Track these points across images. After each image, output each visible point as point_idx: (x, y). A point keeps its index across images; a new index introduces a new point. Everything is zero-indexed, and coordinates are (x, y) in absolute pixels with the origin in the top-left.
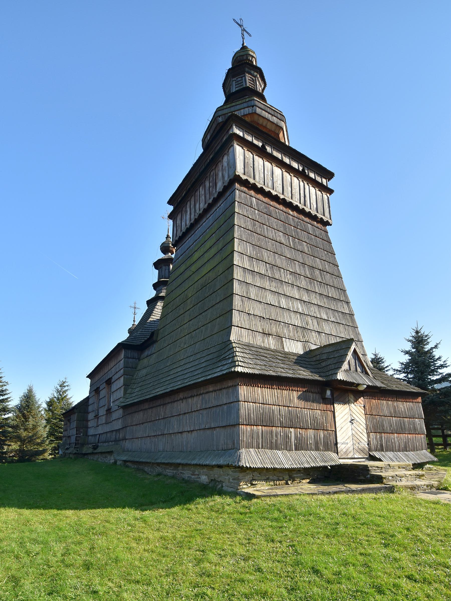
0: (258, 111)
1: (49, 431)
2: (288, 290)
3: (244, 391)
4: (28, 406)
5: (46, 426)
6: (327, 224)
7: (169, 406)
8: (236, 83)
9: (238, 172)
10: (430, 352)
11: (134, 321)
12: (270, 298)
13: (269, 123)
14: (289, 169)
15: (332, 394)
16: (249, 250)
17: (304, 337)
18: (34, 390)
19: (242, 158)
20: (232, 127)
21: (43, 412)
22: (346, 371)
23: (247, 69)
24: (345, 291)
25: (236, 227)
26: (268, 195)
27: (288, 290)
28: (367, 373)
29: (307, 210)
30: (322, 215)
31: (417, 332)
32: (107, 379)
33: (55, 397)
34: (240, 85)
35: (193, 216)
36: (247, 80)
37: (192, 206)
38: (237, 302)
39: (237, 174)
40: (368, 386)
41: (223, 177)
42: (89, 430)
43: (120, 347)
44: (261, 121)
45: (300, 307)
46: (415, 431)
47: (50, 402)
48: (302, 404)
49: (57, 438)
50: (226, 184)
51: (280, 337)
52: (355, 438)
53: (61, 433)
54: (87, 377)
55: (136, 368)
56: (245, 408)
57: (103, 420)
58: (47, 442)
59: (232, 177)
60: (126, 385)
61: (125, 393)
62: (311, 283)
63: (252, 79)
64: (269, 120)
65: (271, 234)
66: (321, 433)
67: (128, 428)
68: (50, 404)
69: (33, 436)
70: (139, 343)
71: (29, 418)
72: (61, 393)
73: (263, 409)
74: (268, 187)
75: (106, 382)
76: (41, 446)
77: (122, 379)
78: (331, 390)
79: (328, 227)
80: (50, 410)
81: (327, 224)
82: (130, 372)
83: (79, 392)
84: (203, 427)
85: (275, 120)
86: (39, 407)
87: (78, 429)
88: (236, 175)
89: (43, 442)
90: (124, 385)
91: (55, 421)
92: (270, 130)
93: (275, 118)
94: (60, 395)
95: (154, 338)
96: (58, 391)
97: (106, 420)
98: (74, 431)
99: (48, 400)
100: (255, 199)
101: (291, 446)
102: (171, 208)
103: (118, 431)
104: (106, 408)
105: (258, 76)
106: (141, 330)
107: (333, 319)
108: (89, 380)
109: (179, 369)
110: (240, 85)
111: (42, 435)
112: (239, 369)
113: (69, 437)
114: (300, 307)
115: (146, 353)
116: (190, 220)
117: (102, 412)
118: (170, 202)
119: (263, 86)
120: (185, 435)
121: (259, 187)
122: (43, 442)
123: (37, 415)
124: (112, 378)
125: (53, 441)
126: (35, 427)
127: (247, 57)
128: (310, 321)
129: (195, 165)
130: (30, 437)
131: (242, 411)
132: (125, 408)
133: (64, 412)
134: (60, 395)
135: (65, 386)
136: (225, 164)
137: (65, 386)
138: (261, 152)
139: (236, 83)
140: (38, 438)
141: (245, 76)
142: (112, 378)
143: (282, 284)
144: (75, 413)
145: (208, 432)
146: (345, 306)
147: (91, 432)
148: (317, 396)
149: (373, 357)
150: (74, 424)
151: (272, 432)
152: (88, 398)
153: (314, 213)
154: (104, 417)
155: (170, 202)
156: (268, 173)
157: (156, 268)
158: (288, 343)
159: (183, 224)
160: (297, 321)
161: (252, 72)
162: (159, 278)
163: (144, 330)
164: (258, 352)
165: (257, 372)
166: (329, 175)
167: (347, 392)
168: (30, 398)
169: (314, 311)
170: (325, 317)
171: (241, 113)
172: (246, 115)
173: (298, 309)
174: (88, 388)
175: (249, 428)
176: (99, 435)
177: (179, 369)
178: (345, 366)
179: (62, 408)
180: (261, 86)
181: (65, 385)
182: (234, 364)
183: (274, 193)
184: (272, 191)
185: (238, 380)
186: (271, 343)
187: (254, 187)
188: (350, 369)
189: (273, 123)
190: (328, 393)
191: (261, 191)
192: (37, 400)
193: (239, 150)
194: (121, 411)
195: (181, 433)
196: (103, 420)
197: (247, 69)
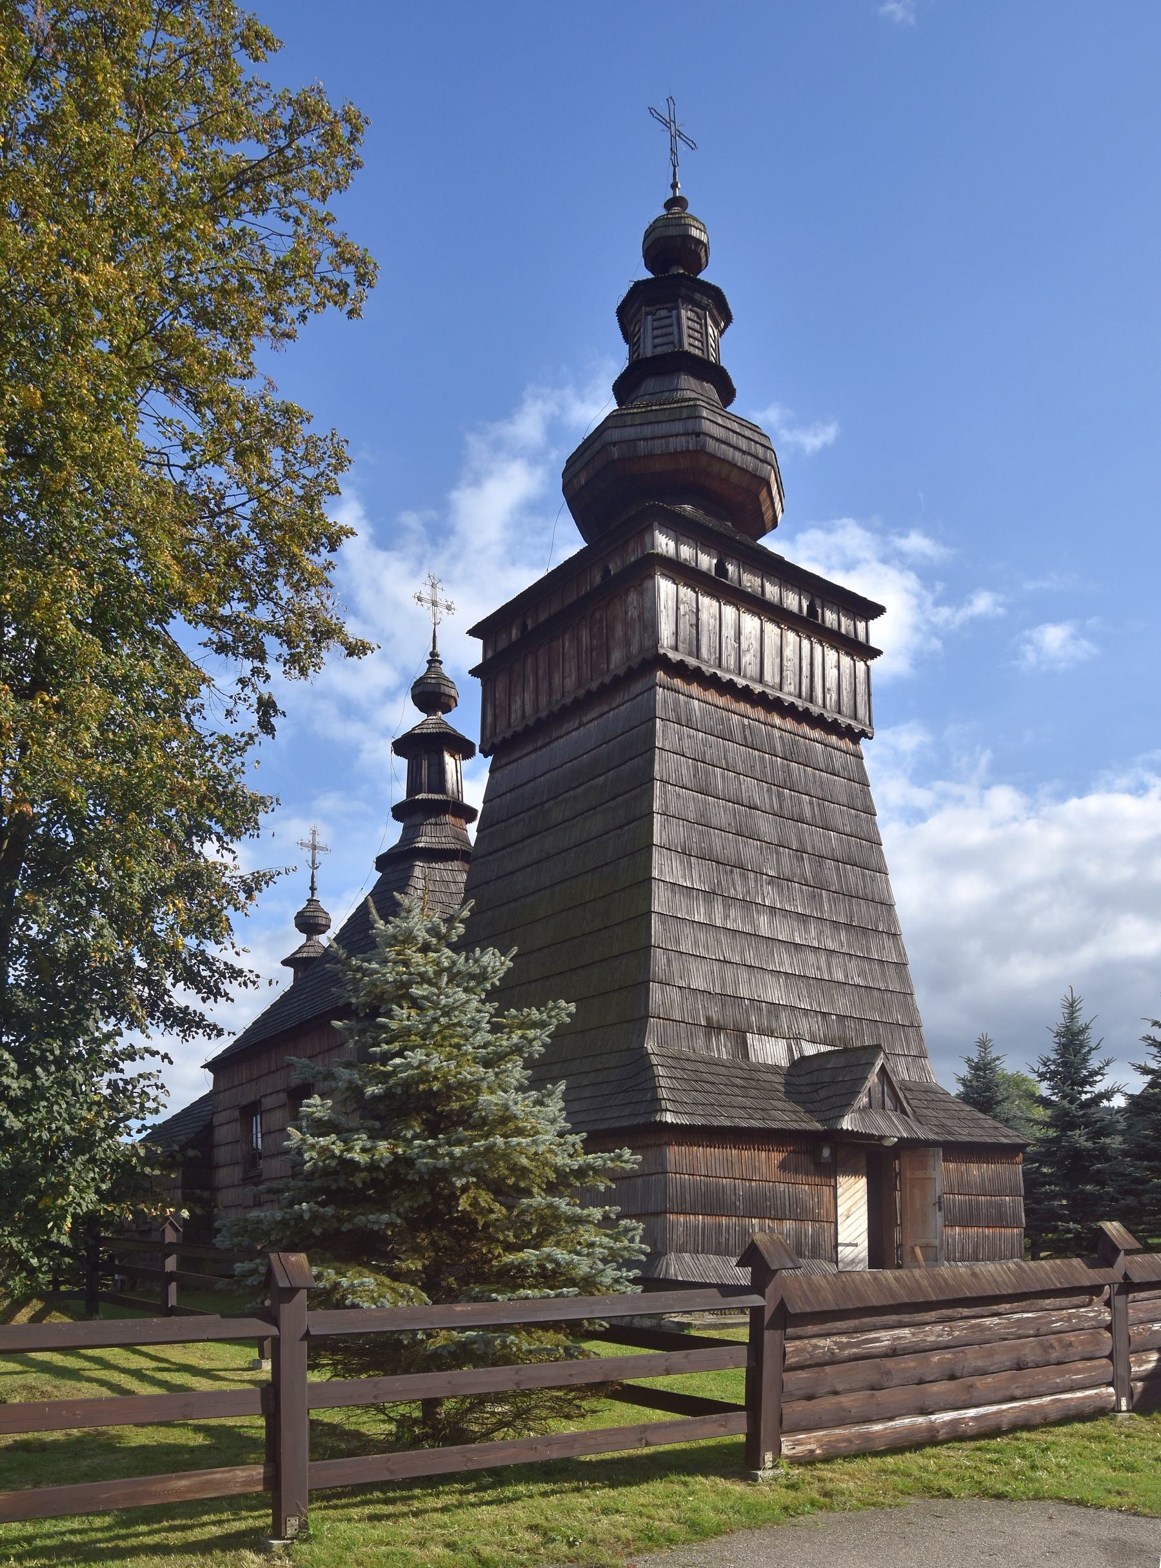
0: (711, 445)
6: (855, 736)
8: (656, 324)
9: (662, 647)
10: (1082, 1031)
11: (313, 889)
15: (834, 1154)
19: (672, 604)
22: (862, 1110)
23: (683, 291)
24: (890, 906)
28: (904, 1112)
29: (815, 710)
30: (850, 718)
34: (664, 331)
35: (543, 700)
36: (684, 321)
37: (541, 672)
39: (661, 651)
40: (901, 1139)
41: (628, 643)
46: (1000, 1220)
50: (635, 663)
64: (732, 465)
66: (809, 1228)
73: (706, 1185)
74: (728, 671)
78: (831, 1148)
85: (749, 463)
93: (749, 458)
100: (699, 702)
110: (664, 331)
112: (669, 1118)
116: (536, 708)
121: (708, 674)
131: (671, 1190)
136: (633, 613)
139: (656, 324)
141: (677, 308)
146: (888, 943)
153: (830, 716)
156: (728, 632)
159: (517, 706)
162: (413, 788)
164: (697, 1073)
165: (699, 1121)
170: (839, 976)
171: (668, 444)
172: (682, 452)
175: (682, 1218)
182: (655, 1105)
183: (741, 682)
184: (735, 679)
186: (721, 1049)
189: (745, 471)
190: (826, 1152)
193: (666, 588)
197: (683, 291)
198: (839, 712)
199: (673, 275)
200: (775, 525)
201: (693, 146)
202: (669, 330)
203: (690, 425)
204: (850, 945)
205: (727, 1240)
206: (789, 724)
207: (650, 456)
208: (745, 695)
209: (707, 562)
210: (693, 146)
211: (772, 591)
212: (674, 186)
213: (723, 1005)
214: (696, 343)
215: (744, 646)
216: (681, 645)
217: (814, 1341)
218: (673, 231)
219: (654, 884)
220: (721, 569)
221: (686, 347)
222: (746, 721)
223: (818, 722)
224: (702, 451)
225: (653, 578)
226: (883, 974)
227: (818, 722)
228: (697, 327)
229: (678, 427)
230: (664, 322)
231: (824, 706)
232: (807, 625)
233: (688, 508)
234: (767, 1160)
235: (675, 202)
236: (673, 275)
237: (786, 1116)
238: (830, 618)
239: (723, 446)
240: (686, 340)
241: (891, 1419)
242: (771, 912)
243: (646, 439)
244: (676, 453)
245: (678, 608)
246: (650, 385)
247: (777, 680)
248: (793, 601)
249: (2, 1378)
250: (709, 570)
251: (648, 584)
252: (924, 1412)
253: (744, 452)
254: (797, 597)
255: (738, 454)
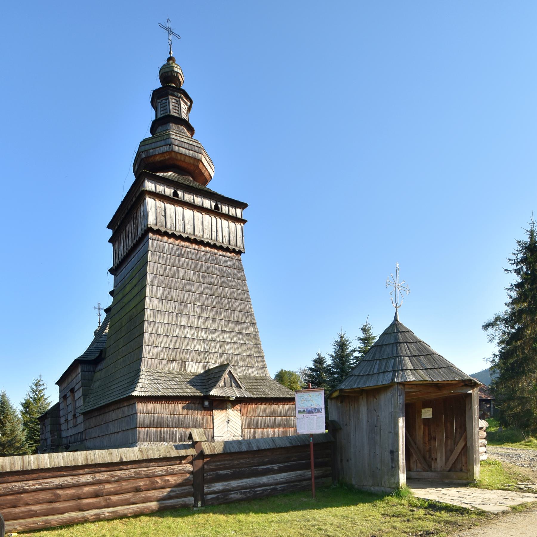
0: (176, 148)
1: (27, 435)
2: (194, 322)
3: (140, 406)
4: (3, 412)
5: (24, 430)
6: (240, 253)
7: (108, 414)
11: (99, 323)
12: (177, 332)
13: (187, 158)
14: (201, 209)
16: (160, 292)
17: (205, 358)
18: (8, 395)
19: (154, 209)
20: (144, 181)
21: (20, 416)
23: (170, 92)
24: (252, 314)
25: (148, 275)
26: (180, 238)
27: (194, 322)
31: (342, 337)
32: (71, 388)
33: (31, 398)
38: (147, 337)
39: (149, 226)
40: (236, 398)
42: (62, 432)
43: (77, 363)
44: (179, 157)
45: (203, 334)
47: (26, 403)
48: (186, 411)
49: (36, 442)
51: (183, 362)
52: (230, 433)
53: (38, 436)
54: (56, 384)
55: (92, 380)
56: (140, 417)
57: (71, 424)
58: (27, 446)
59: (146, 228)
60: (85, 395)
61: (84, 402)
62: (217, 312)
63: (176, 100)
64: (186, 155)
65: (181, 273)
67: (87, 431)
68: (26, 405)
69: (12, 440)
70: (93, 357)
71: (6, 423)
72: (37, 393)
73: (154, 417)
75: (70, 390)
76: (20, 449)
77: (81, 389)
79: (242, 256)
80: (26, 412)
81: (240, 253)
82: (87, 383)
83: (52, 396)
84: (123, 429)
85: (191, 153)
86: (14, 412)
87: (52, 432)
88: (148, 228)
89: (22, 446)
90: (83, 395)
91: (32, 425)
92: (189, 164)
94: (37, 395)
95: (103, 356)
96: (34, 391)
97: (74, 424)
98: (49, 435)
99: (24, 402)
100: (167, 243)
101: (176, 439)
102: (110, 233)
103: (81, 433)
104: (72, 414)
105: (182, 96)
106: (96, 344)
107: (235, 341)
108: (58, 387)
109: (115, 386)
110: (164, 108)
111: (20, 439)
113: (46, 439)
114: (203, 334)
115: (99, 367)
117: (70, 417)
118: (109, 227)
119: (189, 104)
120: (116, 434)
122: (22, 446)
123: (14, 420)
124: (74, 388)
125: (32, 444)
126: (12, 432)
127: (172, 74)
128: (213, 345)
129: (123, 203)
130: (9, 442)
131: (138, 419)
132: (84, 414)
133: (40, 415)
134: (37, 395)
135: (40, 385)
137: (40, 385)
138: (174, 200)
140: (18, 442)
141: (168, 99)
142: (74, 388)
143: (189, 317)
144: (48, 418)
145: (125, 432)
146: (251, 327)
147: (64, 434)
148: (199, 406)
149: (317, 357)
150: (48, 428)
151: (161, 431)
152: (58, 404)
154: (72, 421)
155: (109, 227)
156: (179, 217)
157: (112, 273)
158: (190, 366)
160: (200, 347)
161: (176, 93)
163: (99, 344)
166: (242, 206)
167: (222, 403)
168: (4, 403)
169: (217, 336)
172: (165, 152)
173: (202, 336)
174: (58, 395)
175: (144, 429)
176: (70, 436)
177: (115, 386)
178: (222, 383)
179: (38, 412)
180: (187, 104)
181: (40, 383)
185: (136, 400)
186: (175, 367)
187: (166, 234)
188: (225, 386)
191: (173, 236)
192: (11, 405)
194: (82, 417)
195: (114, 433)
196: (71, 424)
197: (170, 92)
198: (229, 244)
199: (169, 84)
200: (211, 178)
201: (178, 37)
202: (166, 108)
203: (167, 142)
204: (233, 328)
205: (164, 437)
206: (208, 249)
207: (155, 155)
208: (188, 240)
209: (169, 191)
210: (178, 37)
211: (198, 201)
212: (170, 53)
213: (176, 352)
214: (177, 111)
215: (186, 222)
216: (158, 224)
217: (13, 484)
218: (166, 70)
219: (146, 311)
220: (175, 194)
221: (172, 113)
222: (189, 250)
223: (221, 248)
224: (172, 151)
225: (145, 199)
226: (242, 338)
227: (221, 248)
228: (176, 105)
229: (163, 143)
230: (164, 105)
231: (223, 242)
232: (216, 212)
233: (170, 174)
234: (179, 406)
235: (170, 59)
236: (169, 84)
237: (190, 391)
238: (225, 209)
239: (181, 148)
240: (172, 111)
241: (63, 513)
242: (198, 318)
243: (153, 149)
244: (163, 153)
245: (156, 210)
246: (160, 129)
247: (202, 234)
248: (208, 204)
249: (1, 485)
250: (170, 195)
251: (144, 202)
252: (81, 510)
253: (189, 150)
254: (209, 202)
255: (187, 151)
